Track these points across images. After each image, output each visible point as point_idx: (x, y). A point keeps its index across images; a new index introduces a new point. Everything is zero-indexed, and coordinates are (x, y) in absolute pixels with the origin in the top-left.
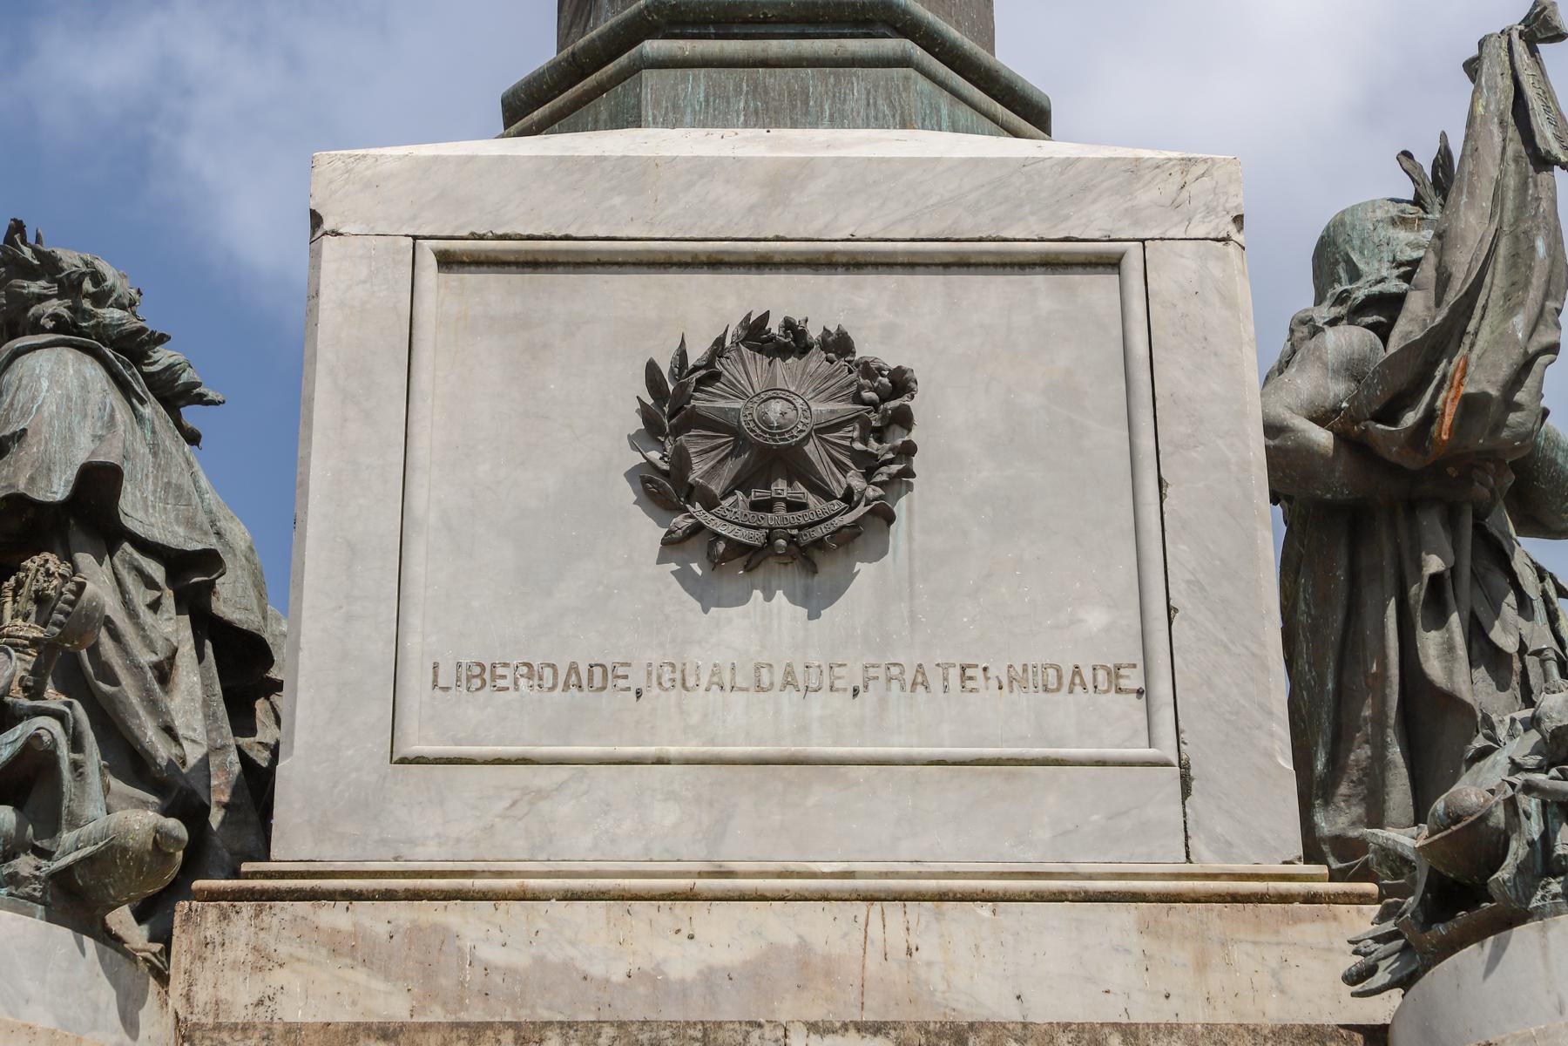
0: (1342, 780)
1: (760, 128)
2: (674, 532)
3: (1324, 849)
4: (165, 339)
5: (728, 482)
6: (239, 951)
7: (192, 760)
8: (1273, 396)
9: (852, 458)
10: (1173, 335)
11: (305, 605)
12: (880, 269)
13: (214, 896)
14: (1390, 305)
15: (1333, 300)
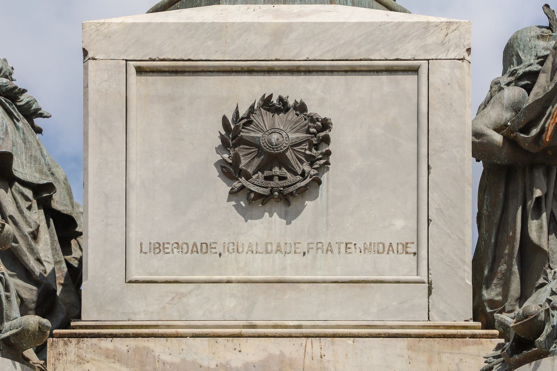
0: (494, 278)
1: (270, 4)
2: (234, 189)
3: (485, 304)
4: (25, 91)
5: (255, 168)
6: (72, 357)
7: (49, 271)
8: (480, 120)
9: (305, 157)
10: (438, 103)
11: (90, 220)
12: (319, 73)
13: (61, 336)
14: (533, 76)
15: (509, 74)
